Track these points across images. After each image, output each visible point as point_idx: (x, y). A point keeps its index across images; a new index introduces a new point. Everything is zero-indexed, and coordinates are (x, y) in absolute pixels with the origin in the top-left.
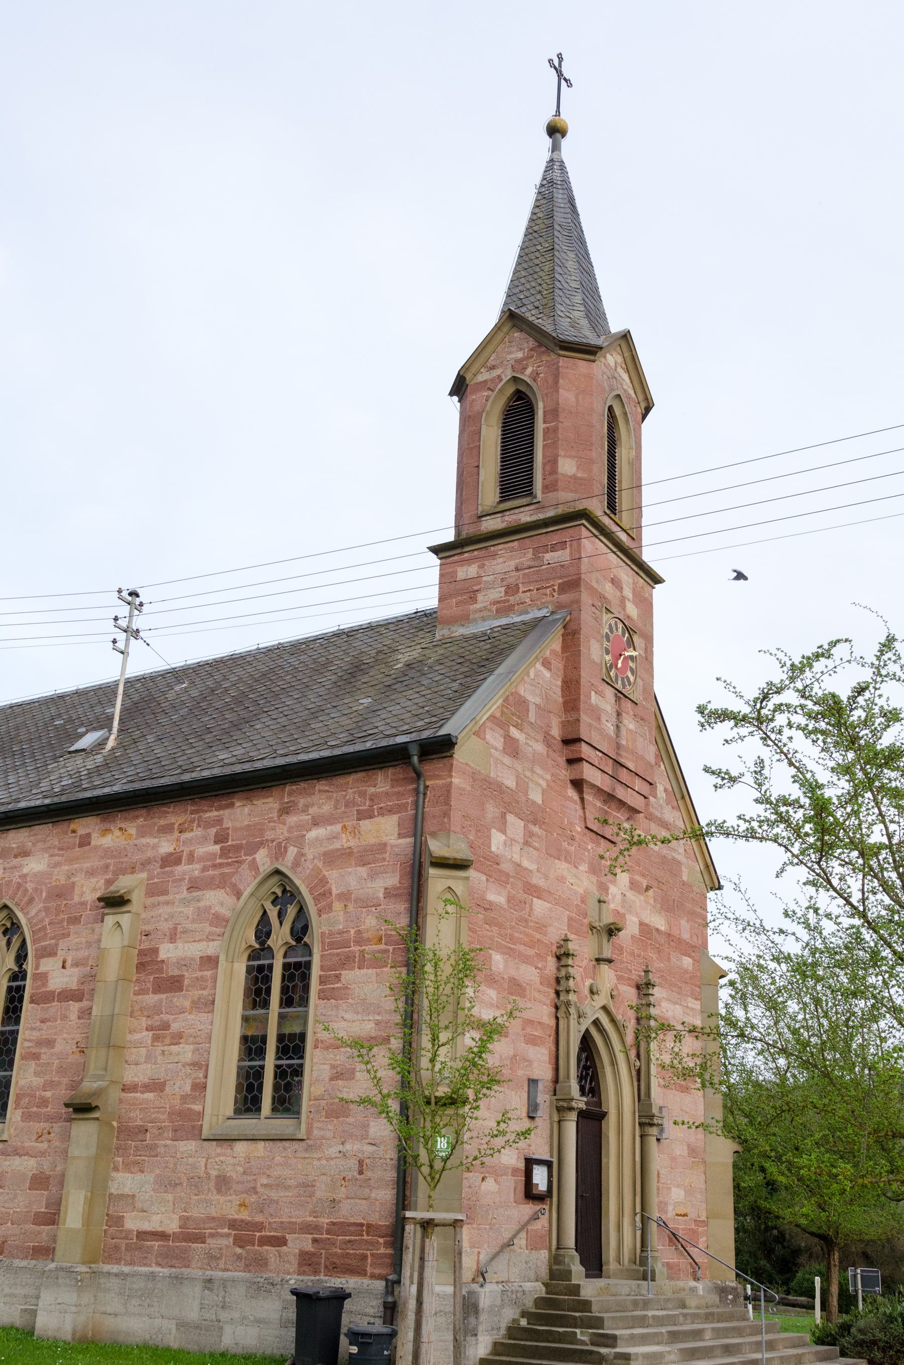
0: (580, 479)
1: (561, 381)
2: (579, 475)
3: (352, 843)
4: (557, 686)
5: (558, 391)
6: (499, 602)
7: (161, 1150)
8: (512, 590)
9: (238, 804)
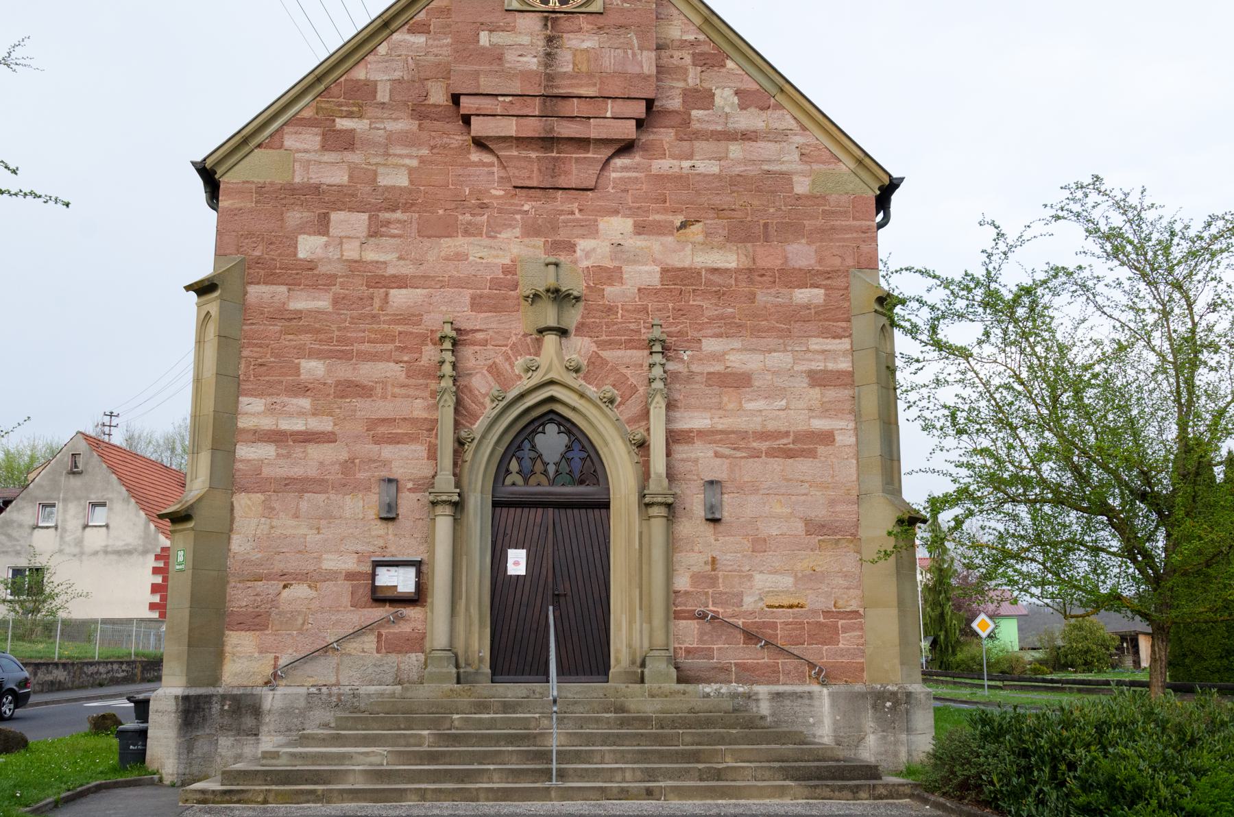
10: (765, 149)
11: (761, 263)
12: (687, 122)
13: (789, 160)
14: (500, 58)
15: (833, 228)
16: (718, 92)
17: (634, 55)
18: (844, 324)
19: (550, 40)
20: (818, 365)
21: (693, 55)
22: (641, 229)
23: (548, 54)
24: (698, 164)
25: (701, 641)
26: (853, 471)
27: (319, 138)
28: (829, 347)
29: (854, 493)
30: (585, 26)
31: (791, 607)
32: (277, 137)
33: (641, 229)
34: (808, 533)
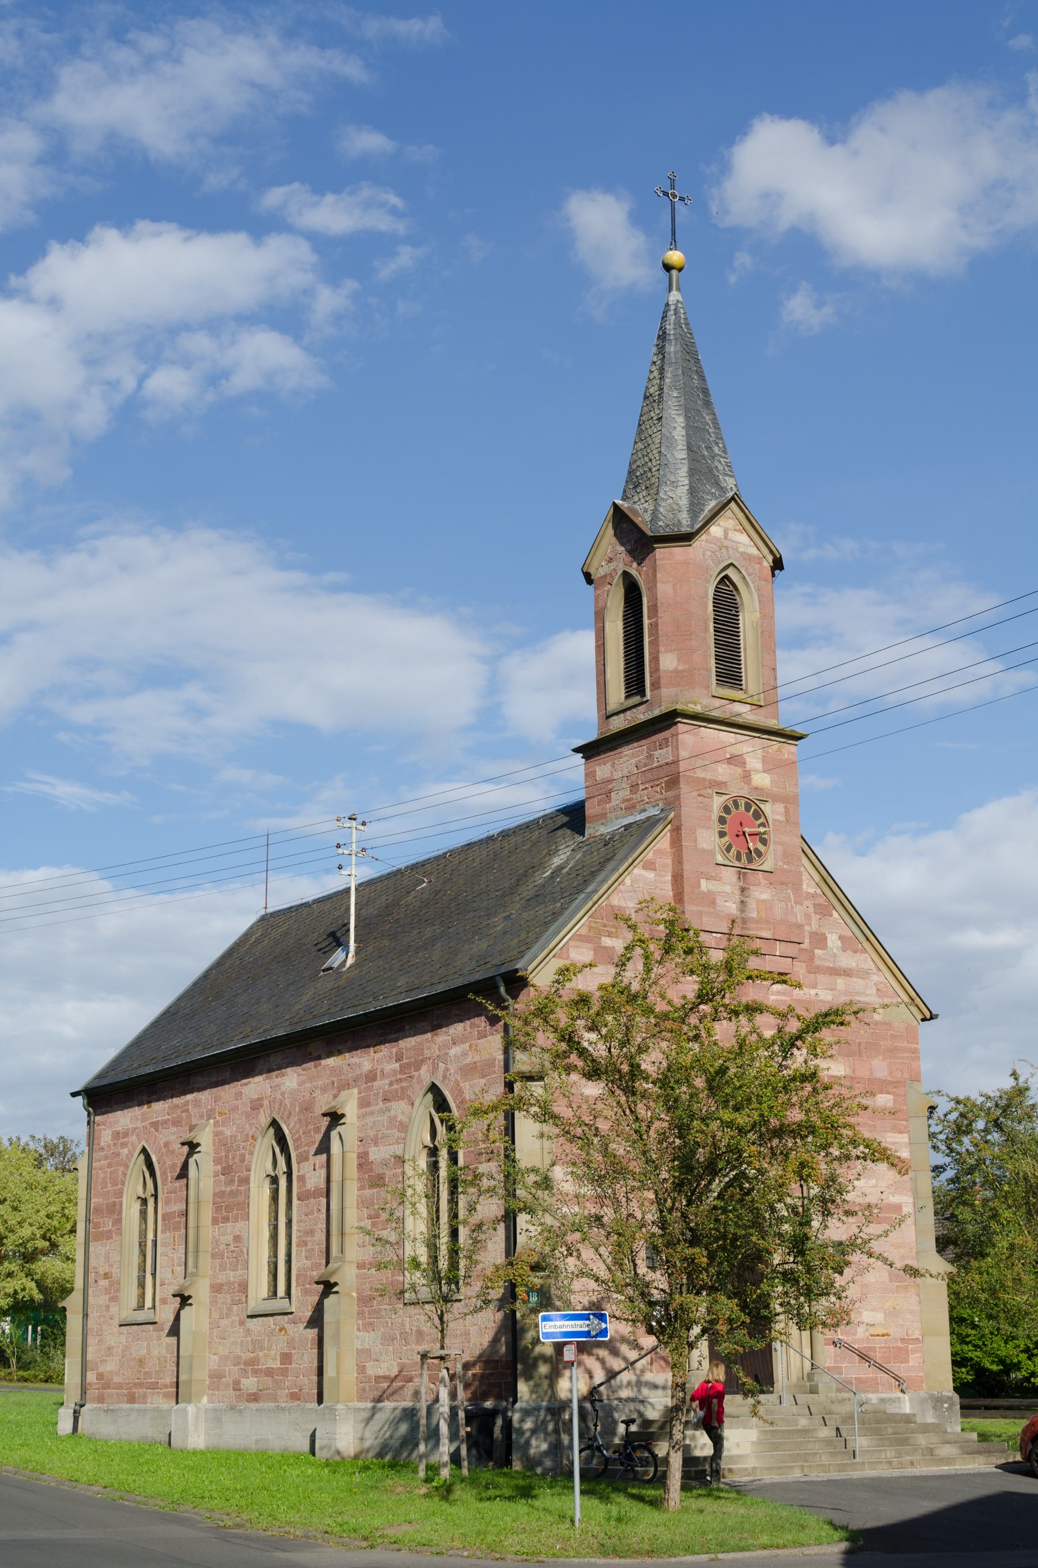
0: (682, 671)
1: (659, 575)
2: (680, 668)
3: (477, 1058)
4: (665, 882)
5: (655, 585)
6: (627, 800)
7: (383, 1313)
8: (634, 788)
9: (407, 1027)
10: (857, 983)
11: (859, 1074)
12: (812, 958)
14: (713, 903)
15: (896, 1049)
16: (828, 936)
17: (792, 907)
18: (904, 1123)
19: (743, 890)
21: (815, 905)
23: (742, 902)
24: (820, 992)
25: (835, 1361)
26: (913, 1233)
27: (592, 953)
28: (896, 1140)
29: (915, 1251)
30: (763, 881)
31: (883, 1335)
32: (564, 949)
34: (891, 1281)
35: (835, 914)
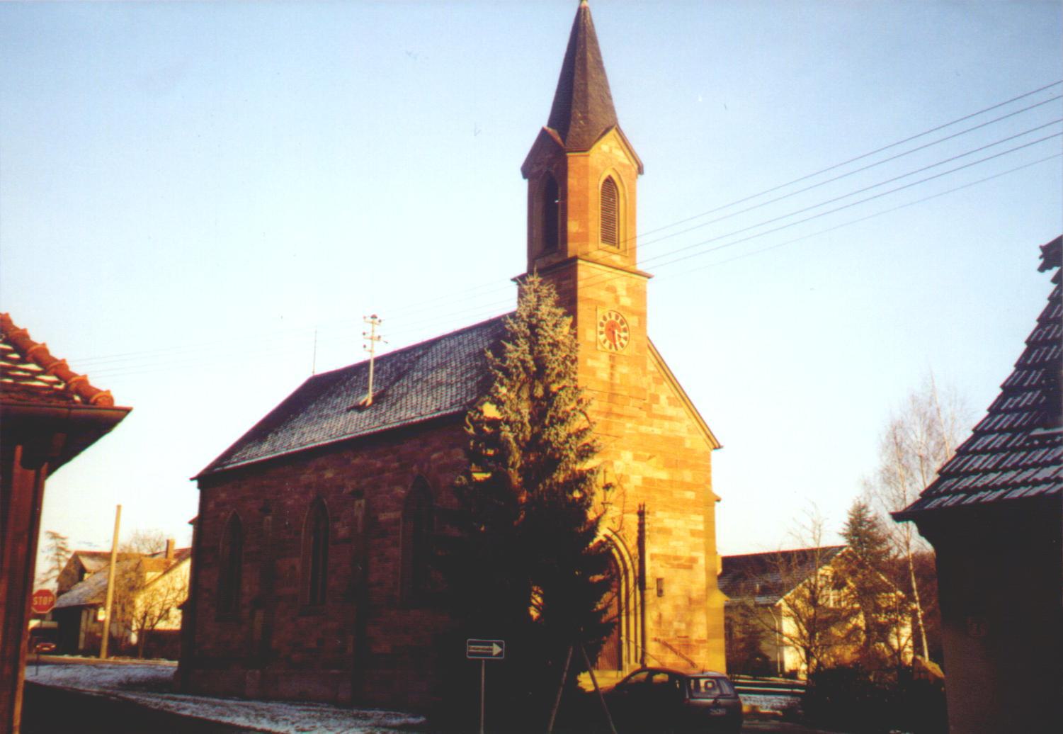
10: (677, 425)
13: (683, 432)
20: (693, 527)
22: (636, 458)
33: (636, 458)
35: (665, 384)
